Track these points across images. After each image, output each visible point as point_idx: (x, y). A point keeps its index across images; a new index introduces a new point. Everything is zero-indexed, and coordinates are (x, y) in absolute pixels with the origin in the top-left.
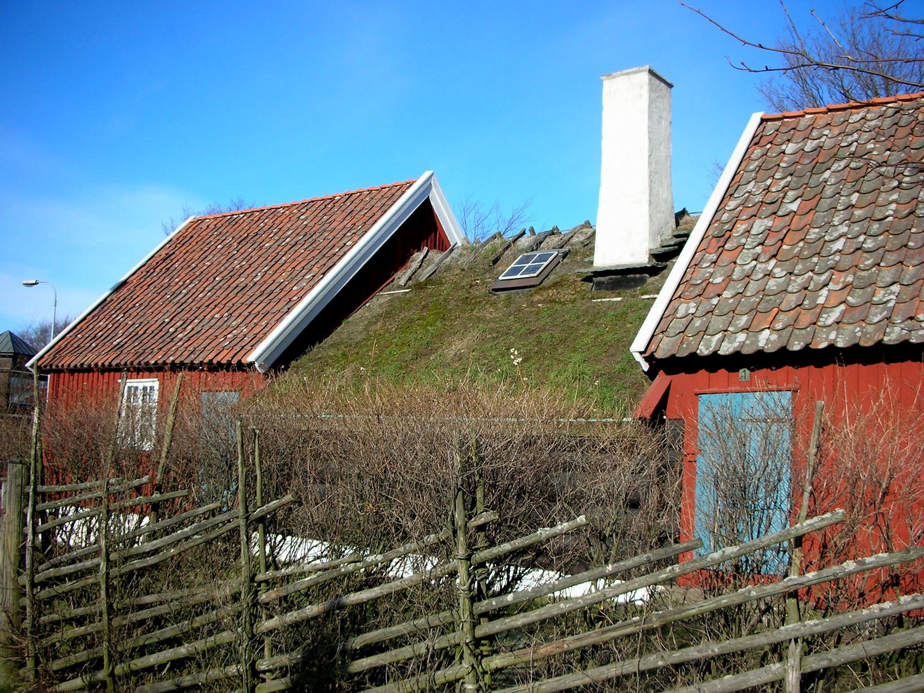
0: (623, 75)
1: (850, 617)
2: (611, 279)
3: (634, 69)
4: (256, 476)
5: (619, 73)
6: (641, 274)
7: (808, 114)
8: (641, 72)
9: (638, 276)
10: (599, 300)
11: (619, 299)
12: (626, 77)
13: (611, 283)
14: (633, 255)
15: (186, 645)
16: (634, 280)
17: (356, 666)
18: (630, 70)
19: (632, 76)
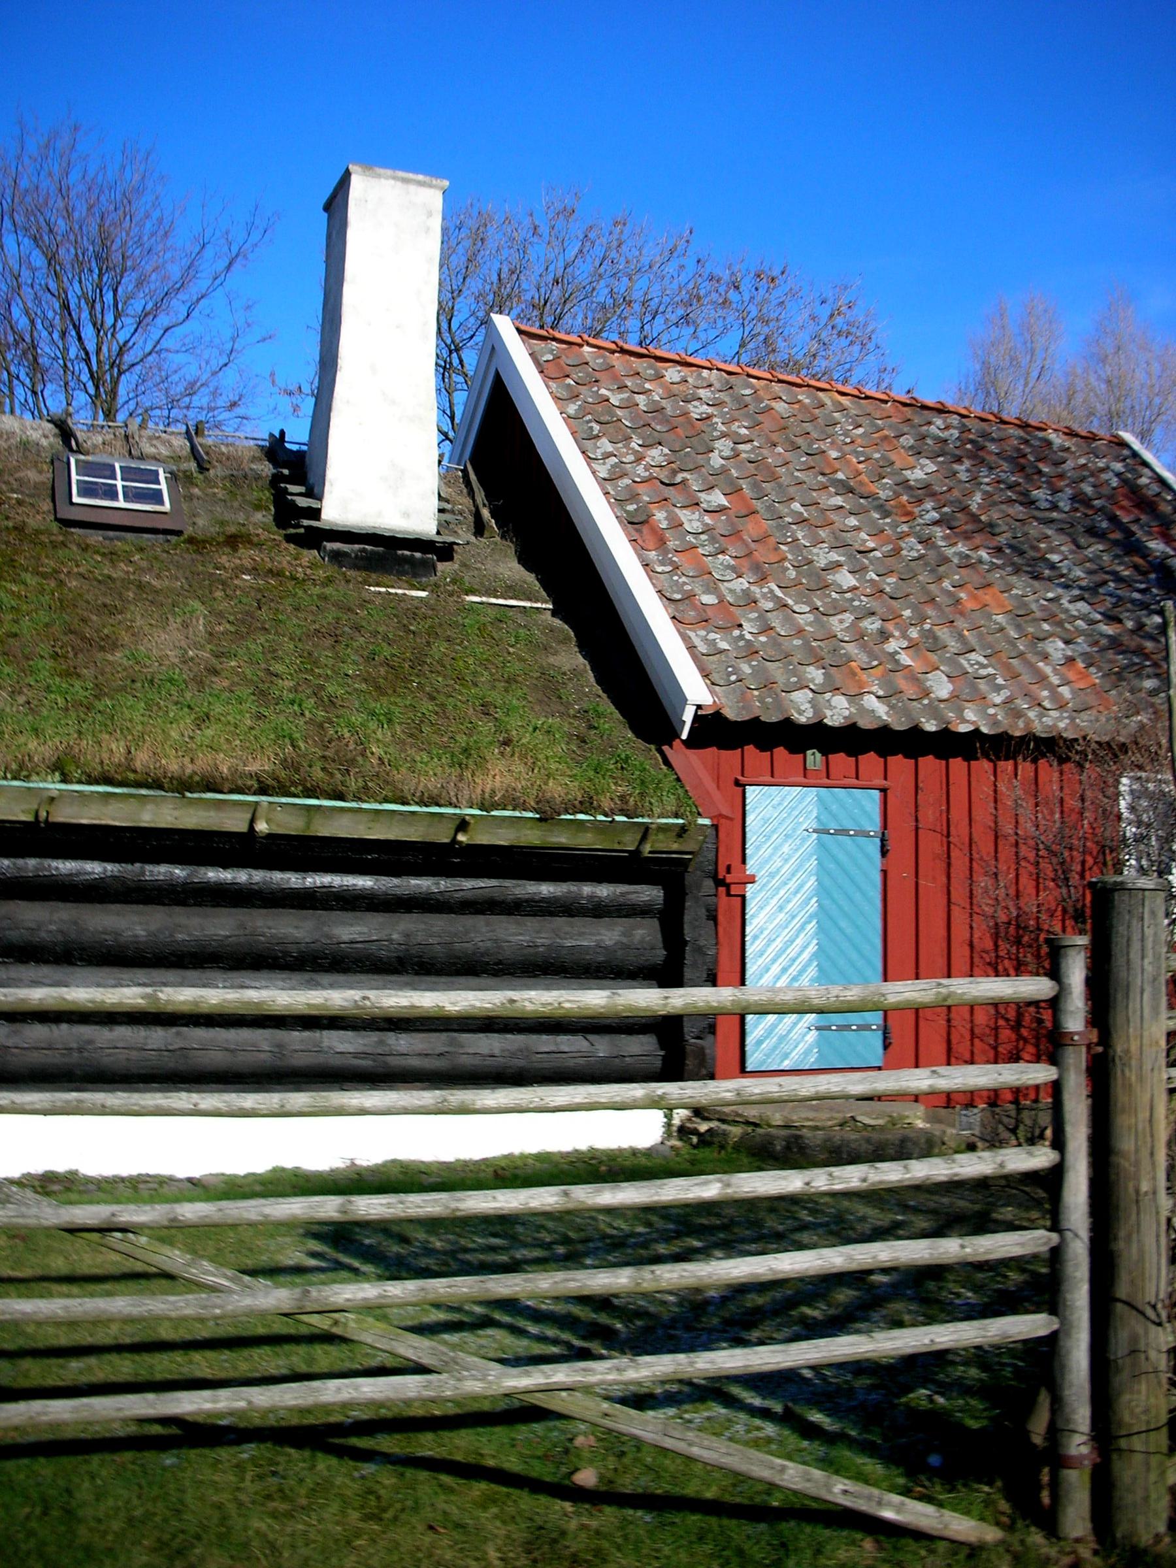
0: (394, 178)
1: (22, 1476)
2: (364, 550)
3: (420, 177)
4: (408, 804)
5: (389, 172)
6: (424, 552)
7: (588, 344)
8: (431, 186)
9: (418, 555)
10: (383, 590)
11: (423, 594)
12: (399, 184)
13: (362, 558)
14: (406, 515)
15: (53, 1265)
16: (410, 561)
17: (1044, 1159)
18: (411, 176)
19: (413, 188)
